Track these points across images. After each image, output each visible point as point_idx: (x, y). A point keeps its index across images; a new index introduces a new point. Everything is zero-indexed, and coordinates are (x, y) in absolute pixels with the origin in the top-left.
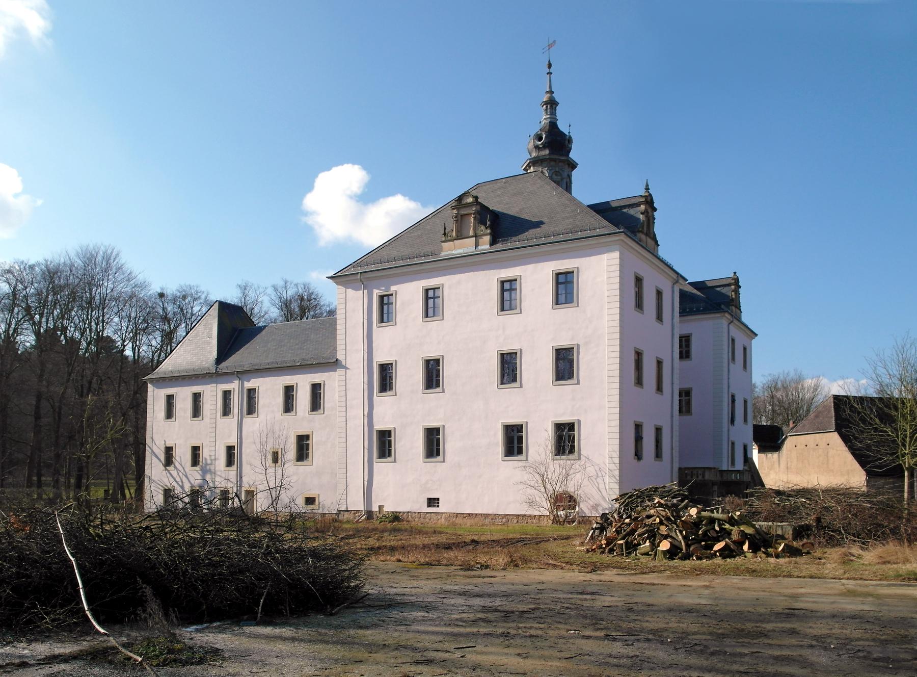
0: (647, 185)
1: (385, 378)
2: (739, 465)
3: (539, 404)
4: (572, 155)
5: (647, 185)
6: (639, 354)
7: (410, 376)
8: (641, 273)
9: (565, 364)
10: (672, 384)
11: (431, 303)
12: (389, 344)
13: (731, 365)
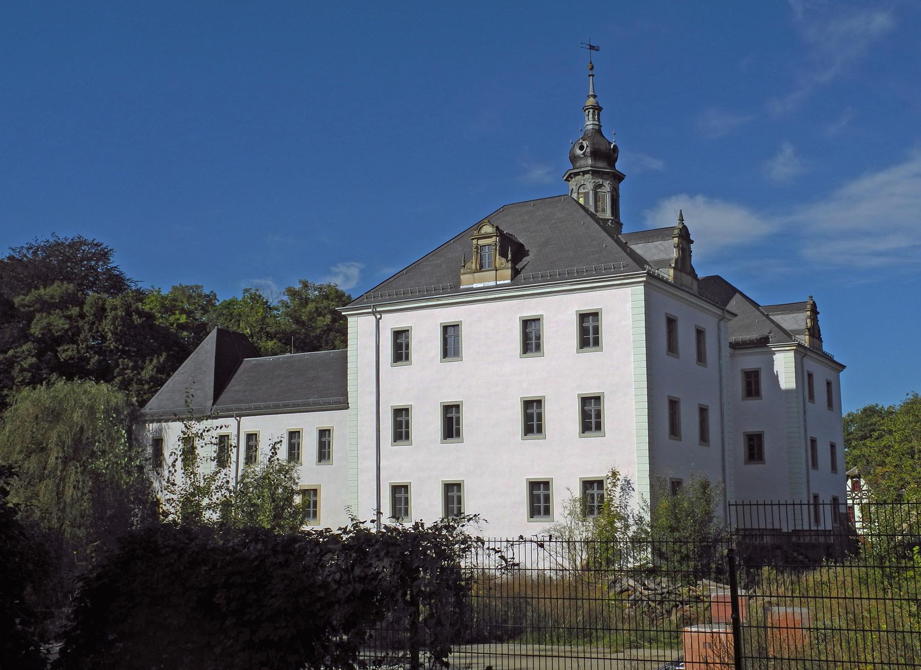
0: (681, 215)
2: (827, 523)
3: (568, 461)
4: (619, 166)
5: (681, 215)
7: (426, 423)
8: (673, 313)
9: (591, 415)
11: (450, 342)
12: (402, 385)
13: (808, 403)
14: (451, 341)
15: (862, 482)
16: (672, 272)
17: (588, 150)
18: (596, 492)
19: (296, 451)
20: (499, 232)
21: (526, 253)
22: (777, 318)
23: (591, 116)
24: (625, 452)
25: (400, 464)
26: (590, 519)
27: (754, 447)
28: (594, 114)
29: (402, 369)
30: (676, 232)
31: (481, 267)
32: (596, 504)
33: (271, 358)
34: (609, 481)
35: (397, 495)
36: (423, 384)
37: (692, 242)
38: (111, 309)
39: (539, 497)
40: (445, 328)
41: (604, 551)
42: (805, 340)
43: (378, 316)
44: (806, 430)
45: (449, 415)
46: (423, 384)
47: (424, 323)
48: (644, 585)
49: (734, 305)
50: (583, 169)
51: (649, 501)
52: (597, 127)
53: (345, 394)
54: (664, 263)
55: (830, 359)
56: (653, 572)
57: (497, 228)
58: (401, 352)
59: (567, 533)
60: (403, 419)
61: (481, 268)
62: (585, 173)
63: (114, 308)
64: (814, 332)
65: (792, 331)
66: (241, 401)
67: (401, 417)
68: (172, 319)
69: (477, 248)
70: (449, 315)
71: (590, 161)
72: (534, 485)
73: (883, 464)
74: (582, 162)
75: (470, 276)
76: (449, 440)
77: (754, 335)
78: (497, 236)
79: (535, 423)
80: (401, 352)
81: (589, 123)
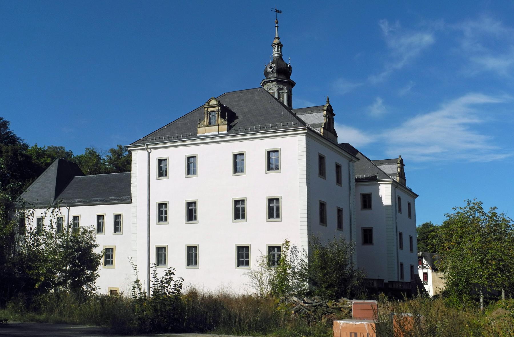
1: (162, 213)
2: (407, 278)
3: (259, 234)
4: (292, 77)
6: (322, 205)
7: (177, 212)
8: (323, 153)
9: (274, 209)
10: (350, 224)
11: (191, 165)
12: (165, 190)
14: (191, 165)
15: (424, 260)
16: (322, 130)
17: (275, 69)
18: (276, 253)
19: (101, 227)
20: (220, 104)
21: (237, 118)
22: (381, 167)
23: (276, 49)
24: (294, 232)
25: (161, 234)
26: (273, 268)
27: (367, 236)
28: (278, 48)
29: (163, 181)
30: (325, 108)
31: (210, 124)
32: (276, 259)
33: (90, 176)
34: (284, 246)
35: (160, 253)
36: (175, 190)
37: (334, 115)
38: (5, 152)
39: (243, 256)
40: (188, 158)
41: (280, 285)
42: (397, 179)
43: (149, 151)
44: (397, 228)
45: (190, 208)
46: (175, 190)
47: (176, 155)
48: (304, 300)
49: (358, 155)
50: (271, 79)
51: (307, 251)
52: (280, 56)
53: (130, 195)
54: (318, 126)
55: (410, 191)
56: (309, 294)
57: (219, 102)
58: (162, 173)
59: (259, 276)
60: (164, 209)
61: (210, 124)
62: (273, 81)
63: (7, 151)
64: (402, 175)
65: (389, 174)
66: (71, 198)
67: (162, 208)
68: (42, 160)
69: (207, 113)
70: (191, 151)
71: (276, 75)
72: (240, 248)
73: (450, 241)
74: (272, 75)
75: (203, 129)
76: (190, 222)
77: (368, 175)
78: (219, 106)
79: (241, 213)
80: (162, 173)
81: (275, 53)
